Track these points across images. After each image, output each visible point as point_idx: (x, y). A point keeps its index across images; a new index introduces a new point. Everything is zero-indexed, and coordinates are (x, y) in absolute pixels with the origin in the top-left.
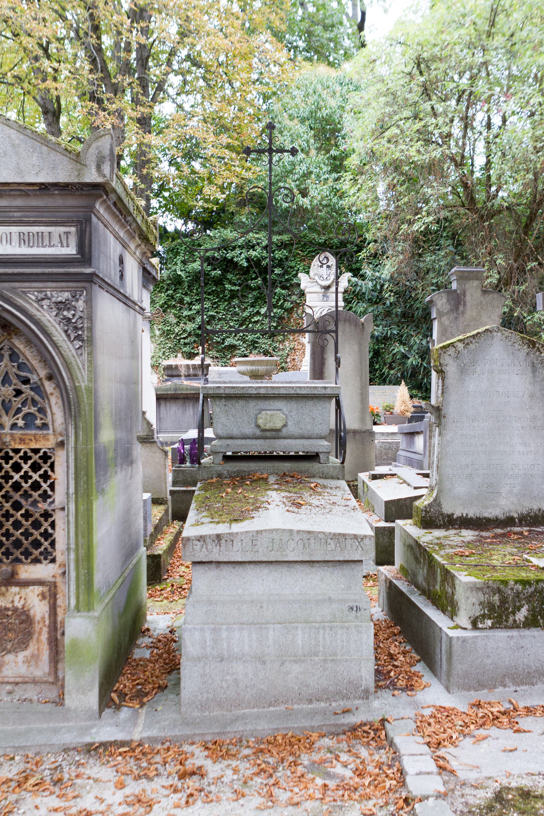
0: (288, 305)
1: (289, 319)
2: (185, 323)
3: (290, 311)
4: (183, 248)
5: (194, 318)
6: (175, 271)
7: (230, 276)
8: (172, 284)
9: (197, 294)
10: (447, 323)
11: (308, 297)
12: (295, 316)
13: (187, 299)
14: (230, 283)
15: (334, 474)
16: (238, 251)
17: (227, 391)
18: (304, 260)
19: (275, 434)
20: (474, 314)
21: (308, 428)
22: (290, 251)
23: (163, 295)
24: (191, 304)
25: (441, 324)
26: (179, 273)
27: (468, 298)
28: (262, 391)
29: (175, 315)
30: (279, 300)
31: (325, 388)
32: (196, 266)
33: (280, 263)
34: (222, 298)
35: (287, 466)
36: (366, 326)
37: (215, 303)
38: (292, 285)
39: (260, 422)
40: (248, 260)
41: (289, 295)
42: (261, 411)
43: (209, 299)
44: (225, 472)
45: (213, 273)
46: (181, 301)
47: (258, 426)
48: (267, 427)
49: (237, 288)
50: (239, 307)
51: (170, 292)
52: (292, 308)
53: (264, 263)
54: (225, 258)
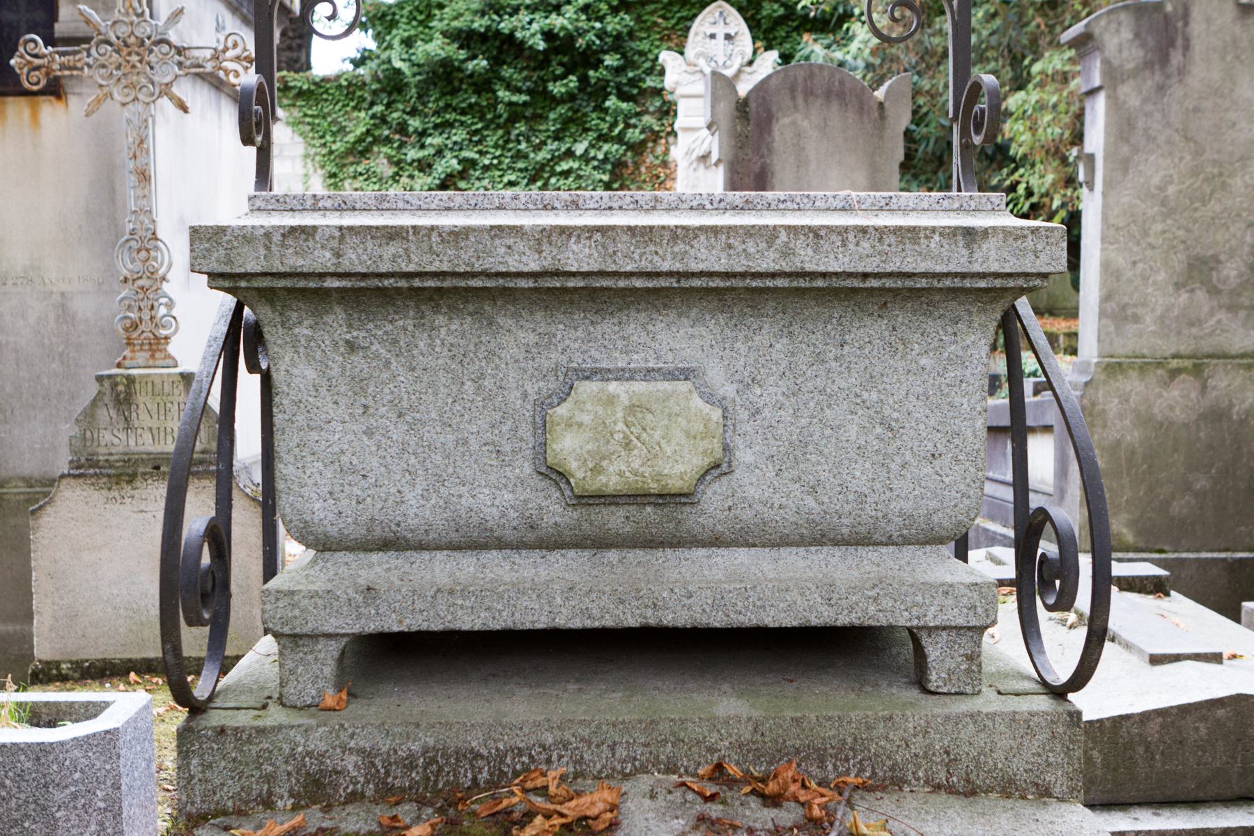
0: (634, 135)
1: (637, 165)
2: (411, 177)
3: (638, 148)
4: (405, 12)
5: (430, 166)
6: (389, 61)
7: (507, 72)
8: (383, 90)
9: (437, 113)
10: (1134, 101)
11: (682, 107)
12: (649, 159)
13: (415, 123)
14: (509, 87)
15: (1018, 766)
16: (524, 16)
17: (356, 259)
18: (669, 38)
19: (659, 516)
20: (1216, 75)
21: (854, 478)
22: (638, 19)
23: (362, 114)
24: (423, 134)
25: (1115, 105)
26: (398, 64)
27: (1197, 27)
28: (580, 257)
29: (389, 158)
30: (614, 125)
31: (970, 234)
32: (435, 48)
33: (617, 43)
34: (492, 121)
35: (727, 711)
36: (890, 110)
37: (476, 132)
38: (643, 92)
39: (569, 447)
40: (548, 35)
41: (638, 114)
42: (570, 380)
43: (462, 123)
44: (350, 762)
45: (470, 66)
46: (402, 129)
47: (555, 475)
48: (611, 480)
49: (524, 98)
50: (528, 140)
51: (378, 109)
52: (643, 143)
53: (581, 42)
54: (498, 33)
